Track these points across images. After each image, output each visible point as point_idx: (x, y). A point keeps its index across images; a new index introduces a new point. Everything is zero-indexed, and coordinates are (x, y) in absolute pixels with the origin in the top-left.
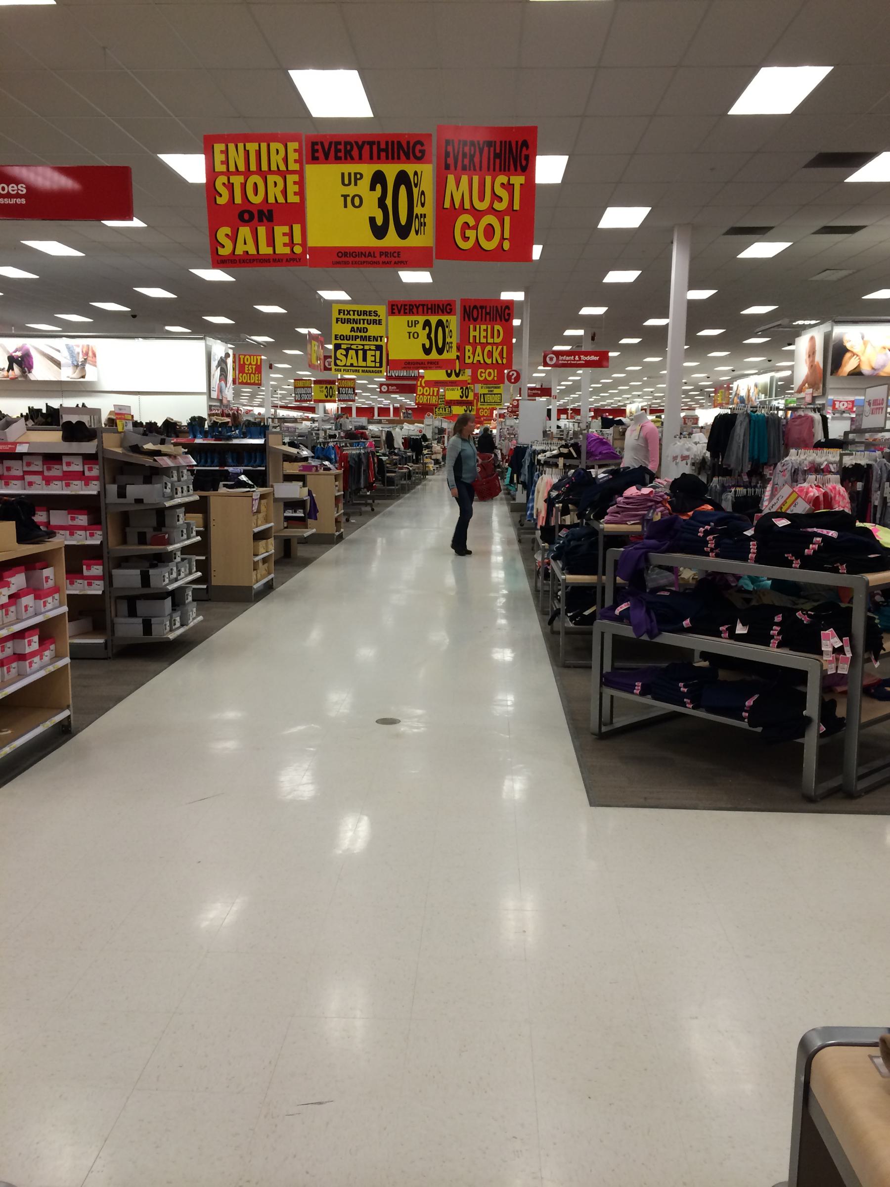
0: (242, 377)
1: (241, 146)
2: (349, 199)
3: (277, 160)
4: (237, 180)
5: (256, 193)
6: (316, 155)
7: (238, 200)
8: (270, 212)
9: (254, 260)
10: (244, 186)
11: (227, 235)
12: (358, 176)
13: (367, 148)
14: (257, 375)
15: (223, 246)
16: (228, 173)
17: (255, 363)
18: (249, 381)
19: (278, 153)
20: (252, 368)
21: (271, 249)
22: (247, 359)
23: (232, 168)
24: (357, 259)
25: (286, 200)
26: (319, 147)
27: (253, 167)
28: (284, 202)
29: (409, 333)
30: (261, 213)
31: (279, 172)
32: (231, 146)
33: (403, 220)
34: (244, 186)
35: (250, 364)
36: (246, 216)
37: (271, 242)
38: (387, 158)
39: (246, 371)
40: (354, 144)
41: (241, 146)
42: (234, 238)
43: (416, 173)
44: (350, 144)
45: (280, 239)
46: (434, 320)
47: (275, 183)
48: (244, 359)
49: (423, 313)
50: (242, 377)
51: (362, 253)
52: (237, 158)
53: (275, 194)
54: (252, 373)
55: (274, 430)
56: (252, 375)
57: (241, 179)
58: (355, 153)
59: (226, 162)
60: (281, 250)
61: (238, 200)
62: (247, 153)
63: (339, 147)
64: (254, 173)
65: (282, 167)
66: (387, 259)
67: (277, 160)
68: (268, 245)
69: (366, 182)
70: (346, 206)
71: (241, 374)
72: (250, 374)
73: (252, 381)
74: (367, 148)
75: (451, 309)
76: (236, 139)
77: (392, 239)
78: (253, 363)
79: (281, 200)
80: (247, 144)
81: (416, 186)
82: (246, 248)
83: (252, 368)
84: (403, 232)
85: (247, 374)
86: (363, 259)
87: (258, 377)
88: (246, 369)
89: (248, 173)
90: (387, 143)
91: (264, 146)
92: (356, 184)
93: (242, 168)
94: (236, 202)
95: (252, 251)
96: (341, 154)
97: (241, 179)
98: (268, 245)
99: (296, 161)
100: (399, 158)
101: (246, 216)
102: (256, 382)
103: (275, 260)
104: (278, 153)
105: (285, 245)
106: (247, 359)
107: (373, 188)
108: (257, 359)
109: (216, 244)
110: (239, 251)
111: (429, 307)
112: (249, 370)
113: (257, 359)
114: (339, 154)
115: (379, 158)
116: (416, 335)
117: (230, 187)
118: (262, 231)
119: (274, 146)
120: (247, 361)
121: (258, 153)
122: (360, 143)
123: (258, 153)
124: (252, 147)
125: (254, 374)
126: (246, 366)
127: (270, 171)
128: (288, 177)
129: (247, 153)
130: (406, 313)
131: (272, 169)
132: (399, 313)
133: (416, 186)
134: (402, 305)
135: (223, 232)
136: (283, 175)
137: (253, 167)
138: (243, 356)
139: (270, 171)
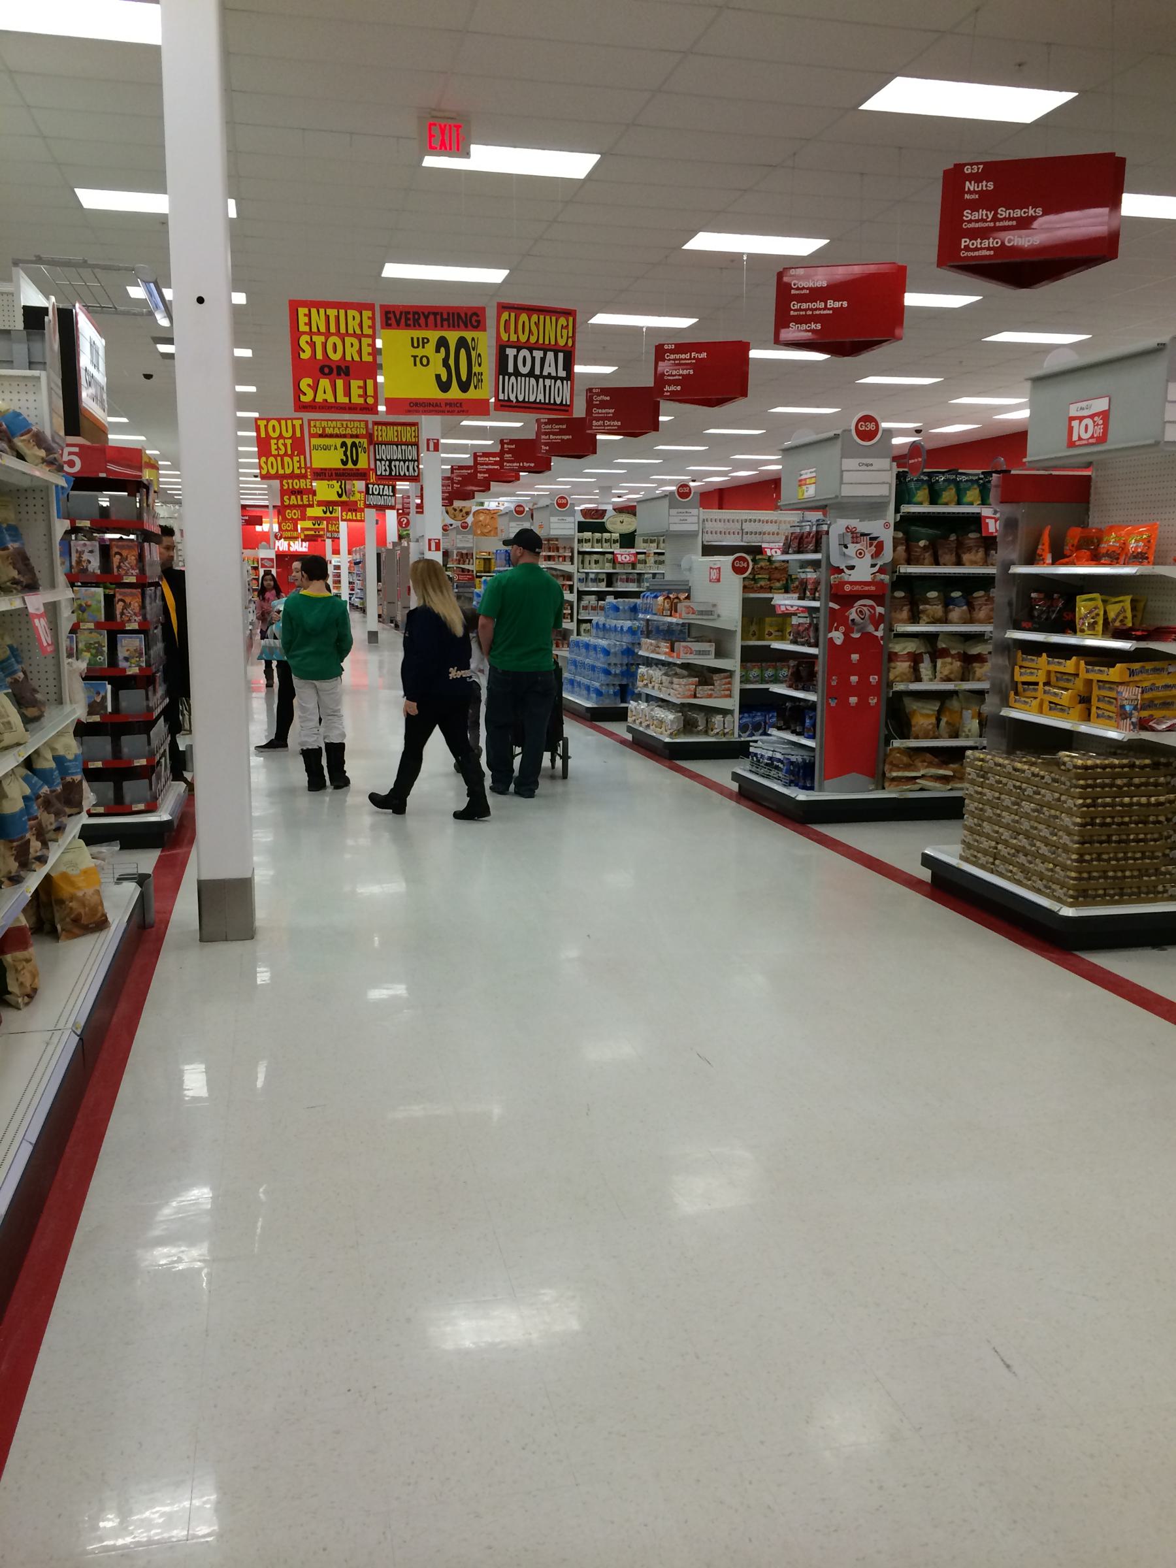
0: (266, 463)
1: (322, 311)
2: (418, 359)
3: (353, 325)
4: (319, 340)
5: (335, 351)
6: (389, 322)
7: (319, 356)
8: (347, 368)
9: (332, 407)
10: (324, 345)
11: (309, 385)
12: (425, 341)
13: (431, 317)
14: (296, 459)
15: (305, 394)
16: (311, 333)
17: (290, 434)
18: (281, 472)
19: (354, 319)
20: (285, 445)
21: (347, 399)
22: (274, 426)
23: (314, 329)
24: (426, 408)
25: (362, 331)
26: (391, 315)
27: (333, 329)
28: (359, 360)
29: (415, 357)
30: (339, 368)
31: (354, 335)
32: (314, 311)
33: (464, 378)
34: (324, 345)
35: (281, 436)
36: (326, 370)
37: (348, 393)
38: (449, 326)
39: (274, 452)
40: (421, 315)
41: (322, 311)
42: (315, 388)
43: (473, 339)
44: (418, 313)
45: (356, 391)
46: (452, 337)
47: (352, 344)
48: (266, 426)
49: (436, 326)
50: (266, 463)
51: (459, 316)
52: (318, 320)
53: (351, 353)
54: (286, 454)
55: (1111, 714)
56: (287, 459)
57: (322, 338)
58: (422, 321)
59: (309, 324)
60: (356, 400)
61: (319, 356)
62: (327, 318)
63: (408, 316)
64: (333, 334)
65: (358, 331)
66: (451, 409)
67: (353, 325)
68: (345, 396)
69: (431, 346)
70: (415, 365)
71: (264, 459)
72: (282, 457)
73: (288, 471)
74: (431, 317)
75: (479, 322)
76: (318, 305)
77: (455, 393)
78: (285, 434)
79: (357, 358)
80: (327, 310)
81: (474, 350)
82: (325, 397)
83: (285, 445)
84: (464, 387)
85: (275, 457)
86: (431, 408)
87: (299, 461)
88: (274, 447)
89: (328, 334)
90: (448, 314)
91: (342, 312)
92: (423, 347)
93: (323, 329)
94: (318, 358)
95: (331, 399)
96: (411, 322)
97: (322, 338)
98: (345, 396)
99: (369, 327)
100: (459, 326)
101: (326, 370)
102: (297, 471)
103: (350, 409)
104: (354, 319)
105: (360, 396)
106: (274, 426)
107: (438, 351)
108: (294, 426)
109: (298, 391)
110: (319, 399)
111: (445, 316)
112: (278, 449)
113: (294, 426)
114: (409, 322)
115: (442, 326)
116: (425, 362)
117: (312, 345)
118: (340, 383)
119: (351, 313)
120: (274, 431)
121: (337, 318)
122: (426, 313)
123: (337, 318)
124: (332, 313)
125: (291, 456)
126: (273, 442)
127: (347, 334)
128: (363, 340)
129: (327, 318)
130: (410, 325)
131: (349, 332)
132: (398, 326)
133: (474, 349)
134: (401, 313)
135: (305, 383)
136: (359, 338)
137: (333, 329)
138: (265, 422)
139: (347, 334)
